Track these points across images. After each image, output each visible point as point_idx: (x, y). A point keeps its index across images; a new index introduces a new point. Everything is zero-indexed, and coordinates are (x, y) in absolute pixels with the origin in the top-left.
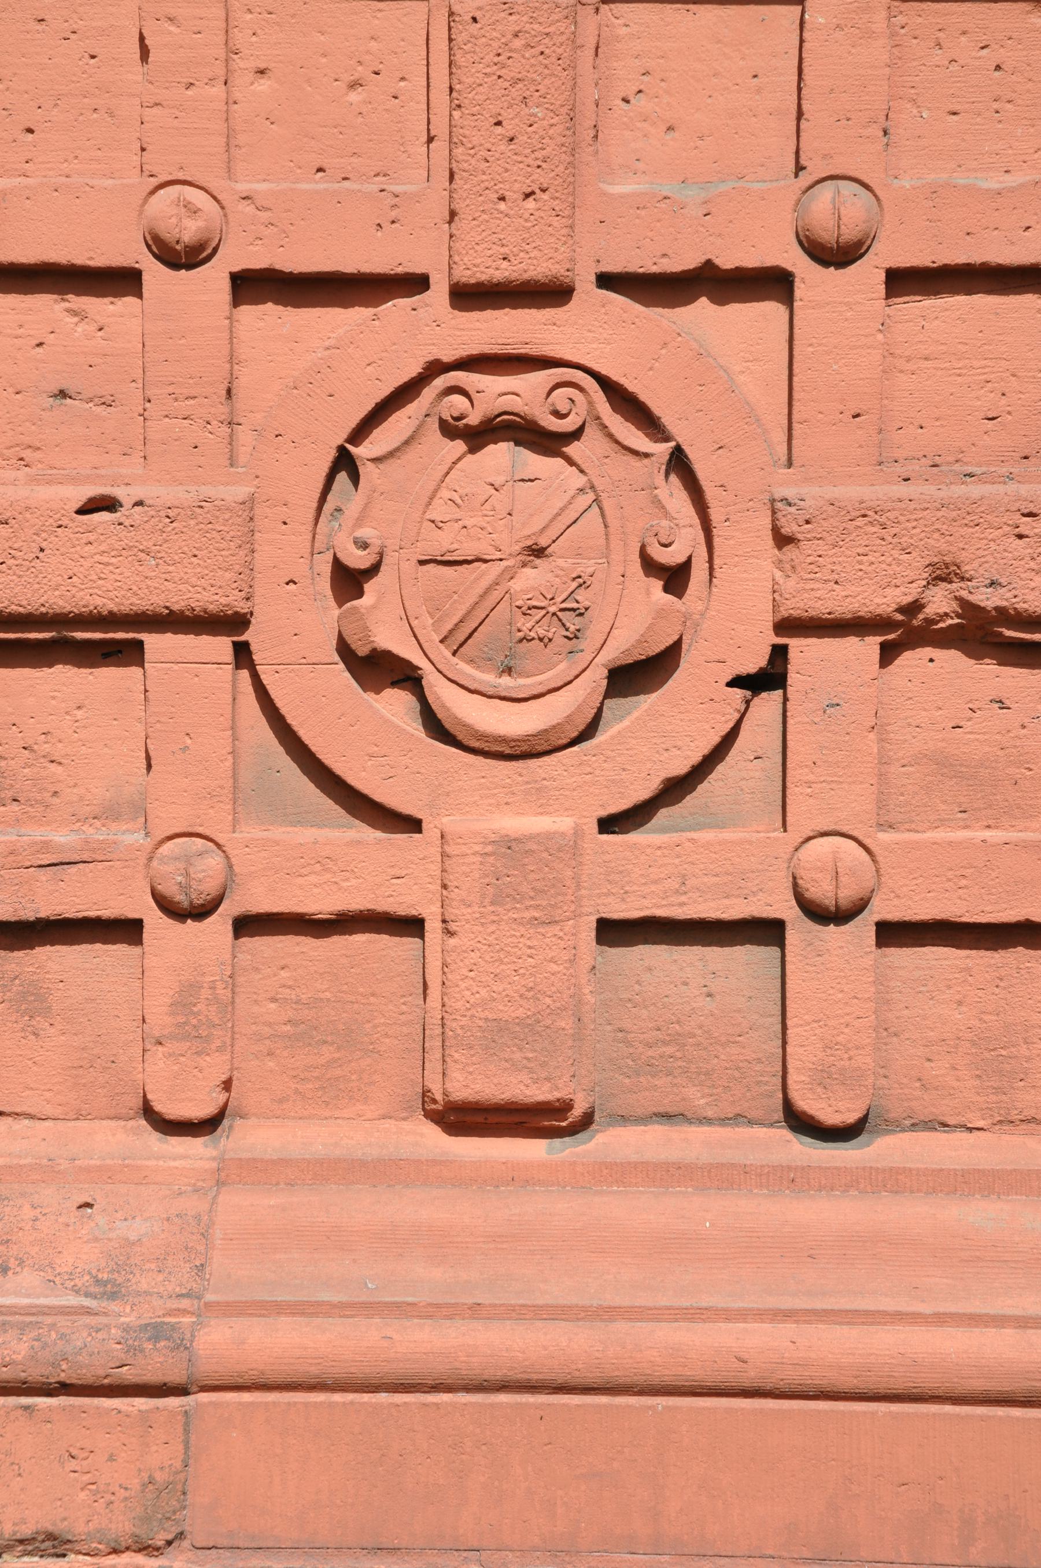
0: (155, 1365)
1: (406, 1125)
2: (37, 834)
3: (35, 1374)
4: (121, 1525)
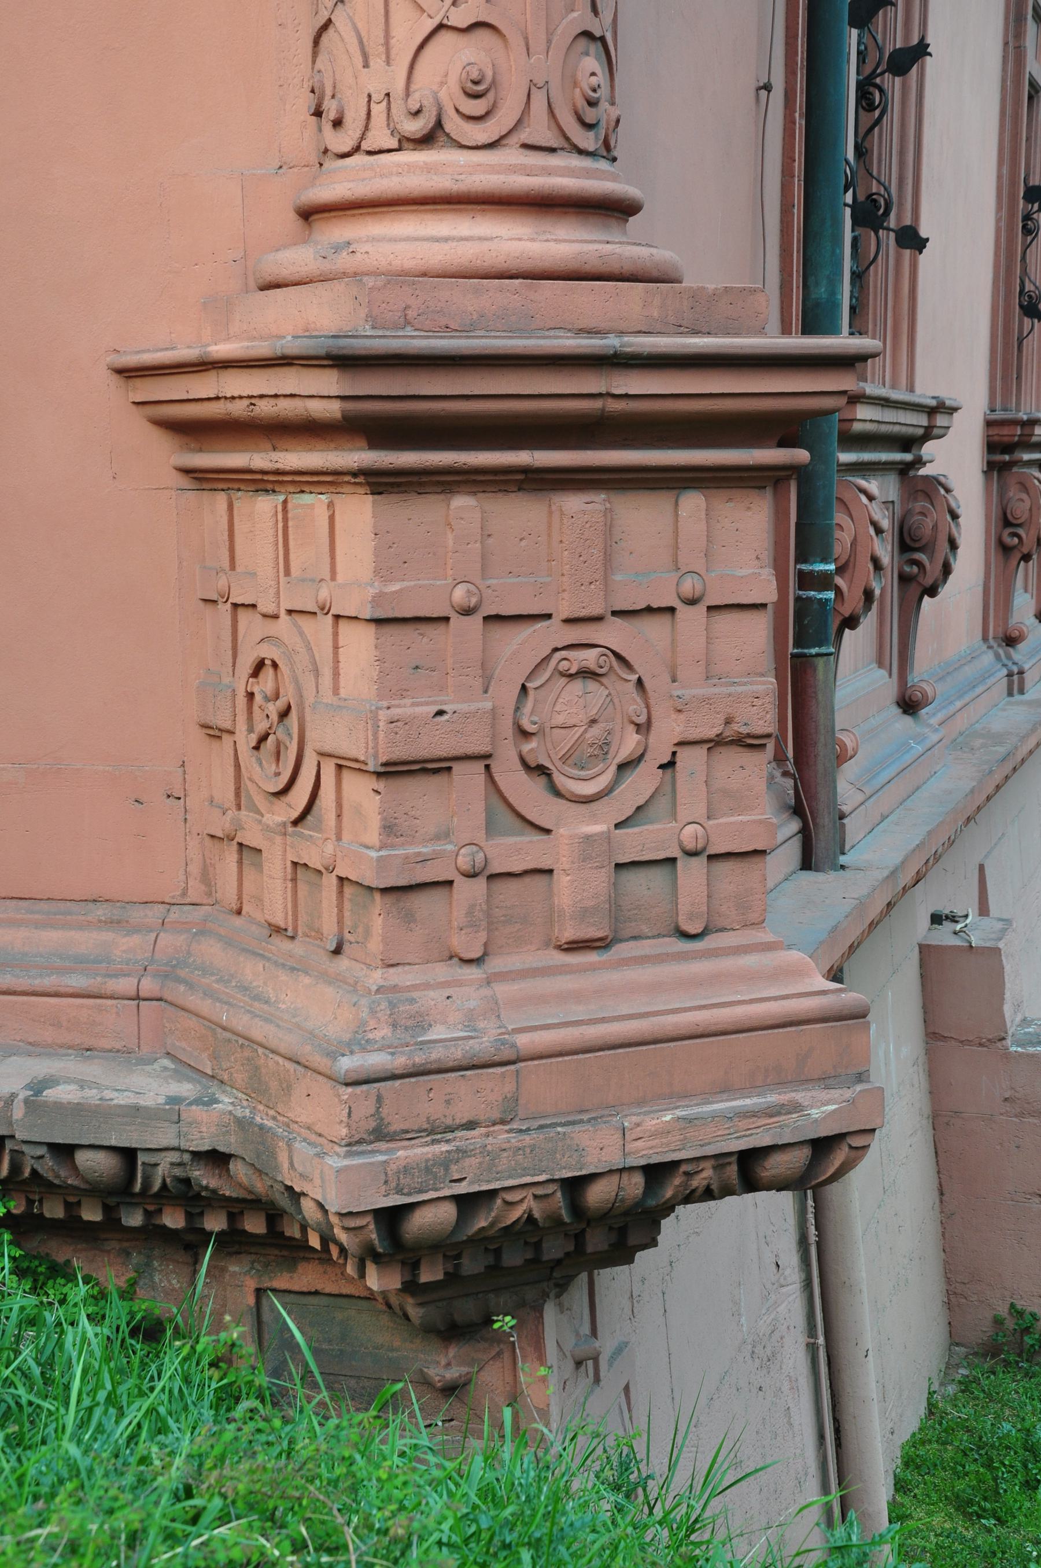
0: (507, 1054)
1: (546, 952)
2: (412, 850)
3: (464, 1063)
4: (496, 1115)
